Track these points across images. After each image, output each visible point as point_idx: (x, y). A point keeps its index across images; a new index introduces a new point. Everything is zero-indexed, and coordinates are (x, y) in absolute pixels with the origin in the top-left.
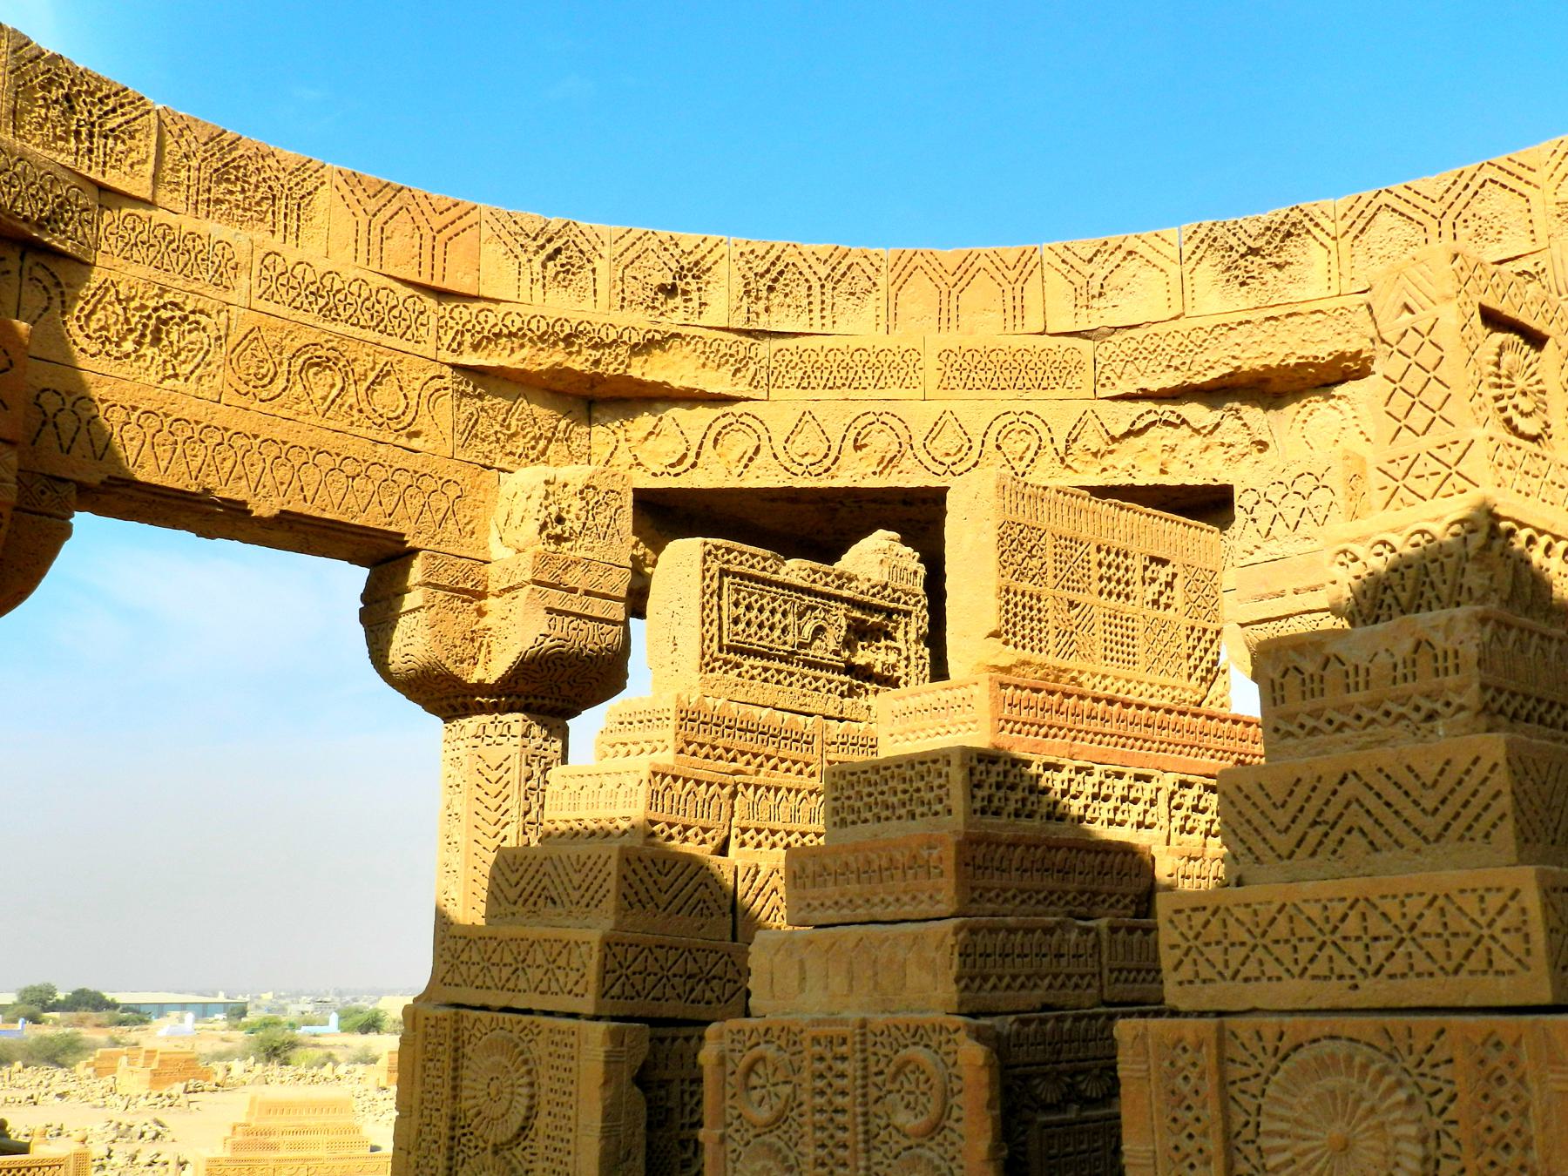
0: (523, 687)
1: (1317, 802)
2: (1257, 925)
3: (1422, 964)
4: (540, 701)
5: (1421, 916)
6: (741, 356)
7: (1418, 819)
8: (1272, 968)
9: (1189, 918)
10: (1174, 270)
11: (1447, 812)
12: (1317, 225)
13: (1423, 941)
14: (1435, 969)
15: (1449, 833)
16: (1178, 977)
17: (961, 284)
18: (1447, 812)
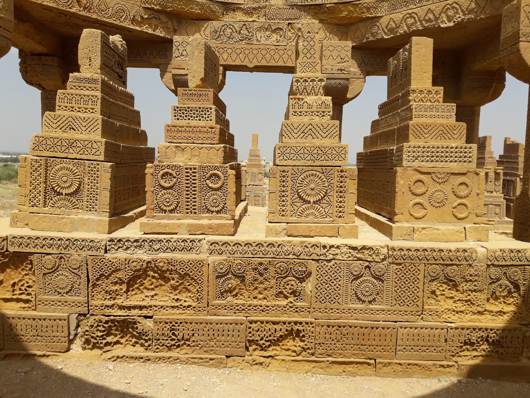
1: (303, 129)
3: (327, 159)
7: (322, 134)
8: (299, 158)
11: (327, 133)
16: (280, 159)
18: (327, 133)
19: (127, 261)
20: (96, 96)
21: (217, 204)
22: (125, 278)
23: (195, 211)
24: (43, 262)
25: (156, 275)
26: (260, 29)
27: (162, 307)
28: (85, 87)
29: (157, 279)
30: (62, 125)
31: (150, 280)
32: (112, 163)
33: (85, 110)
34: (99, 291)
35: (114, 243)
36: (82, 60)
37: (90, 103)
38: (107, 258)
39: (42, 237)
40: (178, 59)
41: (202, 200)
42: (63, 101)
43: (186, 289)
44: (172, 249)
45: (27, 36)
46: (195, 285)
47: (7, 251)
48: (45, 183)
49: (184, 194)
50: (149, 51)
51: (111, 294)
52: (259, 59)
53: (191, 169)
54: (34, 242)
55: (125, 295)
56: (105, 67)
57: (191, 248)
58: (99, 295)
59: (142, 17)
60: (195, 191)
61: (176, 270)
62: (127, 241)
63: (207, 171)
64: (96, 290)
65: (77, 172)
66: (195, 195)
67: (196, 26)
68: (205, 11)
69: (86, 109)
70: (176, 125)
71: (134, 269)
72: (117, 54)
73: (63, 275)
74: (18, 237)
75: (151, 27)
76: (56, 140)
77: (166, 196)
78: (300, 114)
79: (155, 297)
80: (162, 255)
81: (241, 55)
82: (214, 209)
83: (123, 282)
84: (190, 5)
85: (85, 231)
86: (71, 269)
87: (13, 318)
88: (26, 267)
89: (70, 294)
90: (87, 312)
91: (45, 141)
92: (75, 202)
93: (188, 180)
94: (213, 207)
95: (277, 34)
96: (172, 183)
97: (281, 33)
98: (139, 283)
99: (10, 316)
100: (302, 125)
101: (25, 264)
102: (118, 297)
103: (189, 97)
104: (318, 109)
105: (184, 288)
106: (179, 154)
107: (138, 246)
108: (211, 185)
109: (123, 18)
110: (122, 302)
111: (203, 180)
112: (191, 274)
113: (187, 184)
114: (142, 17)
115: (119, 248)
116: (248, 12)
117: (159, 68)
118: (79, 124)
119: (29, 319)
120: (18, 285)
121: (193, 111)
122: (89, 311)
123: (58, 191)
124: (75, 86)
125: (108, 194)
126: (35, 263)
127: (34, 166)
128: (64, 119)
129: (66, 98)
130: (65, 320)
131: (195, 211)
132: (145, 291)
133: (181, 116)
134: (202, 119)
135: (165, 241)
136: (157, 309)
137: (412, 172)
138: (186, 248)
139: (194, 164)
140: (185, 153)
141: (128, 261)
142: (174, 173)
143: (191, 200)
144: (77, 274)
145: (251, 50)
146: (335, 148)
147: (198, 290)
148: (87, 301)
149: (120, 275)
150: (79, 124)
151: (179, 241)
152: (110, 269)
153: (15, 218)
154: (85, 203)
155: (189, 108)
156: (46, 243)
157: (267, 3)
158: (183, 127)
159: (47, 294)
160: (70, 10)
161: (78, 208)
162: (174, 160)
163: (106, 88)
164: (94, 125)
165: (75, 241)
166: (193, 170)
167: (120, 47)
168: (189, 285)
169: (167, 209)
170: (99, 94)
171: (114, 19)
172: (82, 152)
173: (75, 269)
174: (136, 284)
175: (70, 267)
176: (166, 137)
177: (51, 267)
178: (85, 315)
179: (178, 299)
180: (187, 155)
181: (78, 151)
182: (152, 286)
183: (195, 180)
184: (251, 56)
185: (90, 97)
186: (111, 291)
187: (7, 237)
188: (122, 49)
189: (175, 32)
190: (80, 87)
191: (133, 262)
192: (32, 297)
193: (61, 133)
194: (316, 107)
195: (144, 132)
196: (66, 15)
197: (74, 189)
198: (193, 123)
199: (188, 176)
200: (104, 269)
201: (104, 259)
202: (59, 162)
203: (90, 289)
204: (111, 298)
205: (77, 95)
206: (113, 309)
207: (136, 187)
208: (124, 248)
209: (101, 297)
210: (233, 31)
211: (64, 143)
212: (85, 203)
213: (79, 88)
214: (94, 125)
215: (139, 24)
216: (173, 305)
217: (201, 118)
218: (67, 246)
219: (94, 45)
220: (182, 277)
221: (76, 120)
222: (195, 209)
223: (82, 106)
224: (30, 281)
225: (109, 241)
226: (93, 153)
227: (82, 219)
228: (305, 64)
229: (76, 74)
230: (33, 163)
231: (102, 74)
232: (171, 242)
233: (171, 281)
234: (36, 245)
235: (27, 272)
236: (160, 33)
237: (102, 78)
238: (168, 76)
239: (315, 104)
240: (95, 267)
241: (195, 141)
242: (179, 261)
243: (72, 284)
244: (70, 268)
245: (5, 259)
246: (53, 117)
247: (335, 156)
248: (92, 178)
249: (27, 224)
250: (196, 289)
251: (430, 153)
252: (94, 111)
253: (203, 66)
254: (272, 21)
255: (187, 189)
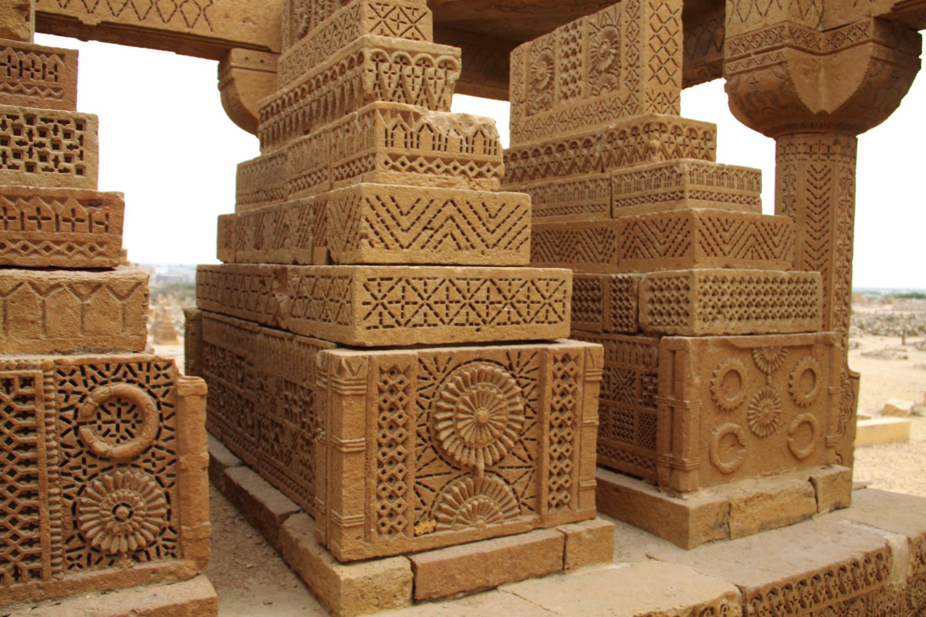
1: (429, 215)
2: (426, 291)
3: (515, 317)
5: (518, 291)
7: (487, 236)
8: (432, 319)
9: (379, 284)
11: (499, 232)
13: (517, 305)
14: (520, 319)
15: (500, 244)
18: (499, 232)
23: (35, 565)
63: (81, 388)
78: (410, 164)
100: (425, 201)
104: (464, 153)
108: (101, 446)
134: (41, 165)
137: (717, 350)
143: (14, 521)
146: (538, 283)
194: (458, 145)
228: (387, 9)
239: (453, 134)
247: (536, 307)
251: (744, 297)
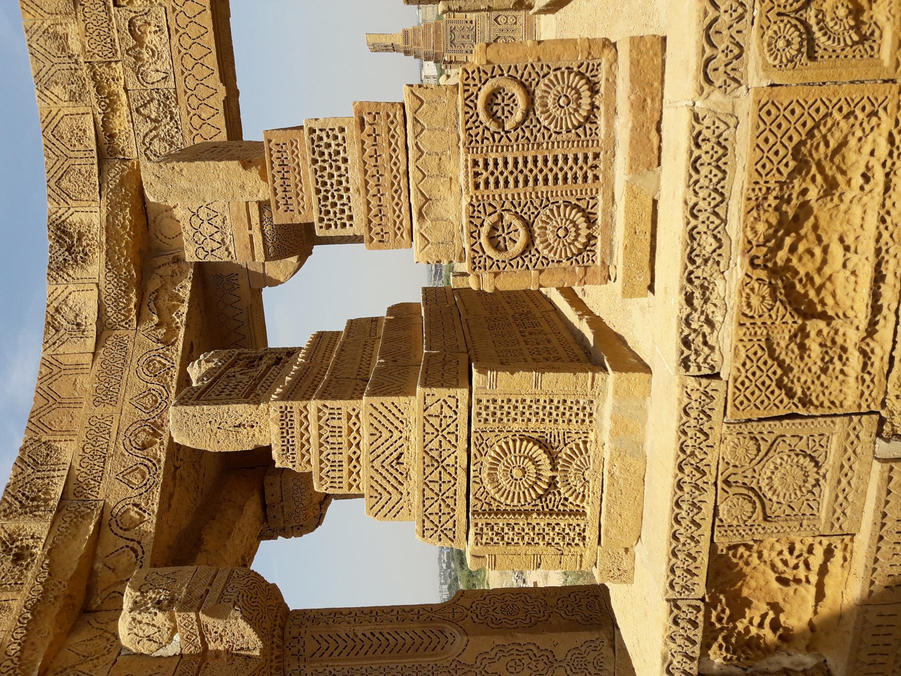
0: (267, 625)
4: (278, 618)
6: (73, 516)
10: (72, 287)
12: (60, 217)
17: (55, 396)
19: (744, 320)
20: (319, 410)
21: (572, 95)
22: (793, 322)
23: (590, 156)
24: (735, 523)
25: (788, 241)
26: (140, 74)
27: (883, 221)
28: (302, 435)
29: (799, 238)
30: (393, 481)
31: (800, 259)
32: (474, 371)
33: (354, 434)
34: (820, 388)
35: (692, 358)
36: (245, 443)
37: (335, 423)
38: (735, 373)
39: (672, 527)
40: (231, 249)
41: (559, 138)
42: (337, 480)
43: (836, 152)
44: (719, 199)
45: (230, 534)
46: (829, 124)
47: (703, 600)
48: (527, 513)
49: (544, 189)
50: (225, 311)
51: (832, 359)
52: (206, 72)
53: (476, 174)
54: (684, 545)
55: (836, 323)
56: (252, 394)
57: (719, 143)
58: (832, 389)
59: (158, 325)
60: (535, 161)
61: (781, 184)
62: (688, 325)
63: (480, 130)
64: (817, 397)
65: (500, 447)
66: (546, 161)
67: (159, 218)
68: (124, 199)
69: (350, 431)
70: (365, 221)
71: (769, 301)
72: (226, 369)
73: (770, 478)
74: (672, 577)
75: (175, 307)
76: (428, 494)
77: (551, 237)
79: (849, 241)
80: (734, 229)
81: (204, 116)
82: (585, 102)
83: (802, 328)
84: (117, 232)
85: (644, 424)
86: (758, 458)
87: (872, 583)
88: (742, 556)
89: (821, 459)
90: (875, 417)
91: (431, 517)
92: (571, 449)
93: (506, 182)
94: (579, 105)
95: (144, 33)
96: (517, 224)
97: (139, 23)
98: (805, 286)
99: (867, 590)
101: (735, 560)
102: (839, 340)
103: (292, 194)
105: (832, 160)
106: (438, 210)
107: (704, 294)
108: (518, 116)
109: (164, 361)
110: (857, 328)
111: (504, 140)
112: (796, 139)
113: (516, 182)
114: (158, 325)
115: (705, 343)
116: (110, 104)
117: (260, 291)
118: (387, 444)
119: (879, 549)
120: (784, 572)
121: (326, 179)
122: (871, 413)
123: (546, 487)
124: (303, 456)
125: (549, 376)
126: (737, 540)
127: (492, 539)
128: (378, 477)
129: (331, 474)
130: (891, 469)
131: (590, 156)
132: (827, 271)
133: (343, 211)
135: (693, 222)
136: (886, 235)
138: (718, 160)
139: (462, 166)
140: (435, 194)
141: (746, 320)
142: (489, 221)
143: (561, 169)
144: (772, 445)
145: (189, 92)
147: (846, 117)
148: (846, 419)
149: (782, 338)
150: (387, 444)
151: (697, 182)
152: (765, 363)
153: (611, 574)
154: (574, 426)
155: (318, 191)
156: (689, 518)
157: (81, 59)
158: (368, 203)
159: (815, 512)
160: (162, 463)
161: (585, 443)
162: (456, 223)
163: (300, 390)
164: (385, 412)
165: (683, 451)
166: (480, 169)
167: (211, 365)
168: (827, 145)
169: (584, 232)
170: (313, 405)
171: (169, 379)
172: (452, 438)
173: (759, 450)
174: (806, 295)
175: (752, 460)
176: (398, 246)
177: (750, 505)
178: (882, 421)
179: (864, 176)
180: (440, 189)
181: (449, 446)
182: (818, 251)
183: (506, 163)
184: (202, 92)
185: (321, 423)
186: (823, 359)
187: (668, 600)
188: (216, 360)
189: (178, 259)
190: (303, 446)
191: (749, 305)
192: (820, 543)
193: (412, 483)
195: (391, 310)
196: (176, 468)
197: (541, 451)
198: (355, 177)
199: (497, 183)
200: (764, 378)
201: (736, 380)
202: (477, 486)
203: (813, 411)
204: (840, 358)
205: (321, 453)
206: (872, 352)
207: (515, 319)
208: (706, 329)
209: (836, 383)
210: (155, 137)
211: (435, 476)
212: (574, 426)
213: (307, 447)
214: (385, 412)
215: (172, 331)
216: (880, 188)
217: (339, 158)
218: (697, 469)
219: (205, 419)
220: (802, 166)
221: (379, 451)
222: (586, 158)
223: (344, 439)
224: (778, 547)
225: (687, 368)
226: (452, 414)
227: (614, 434)
229: (275, 454)
230: (484, 541)
231: (268, 401)
232: (696, 205)
233: (808, 198)
234: (692, 538)
235: (755, 555)
236: (185, 289)
237: (275, 400)
238: (273, 269)
240: (758, 403)
241: (402, 168)
242: (756, 177)
243: (797, 455)
244: (755, 462)
245: (721, 601)
246: (374, 501)
248: (513, 413)
249: (627, 550)
250: (843, 123)
252: (354, 414)
253: (212, 163)
254: (118, 47)
255: (531, 183)
